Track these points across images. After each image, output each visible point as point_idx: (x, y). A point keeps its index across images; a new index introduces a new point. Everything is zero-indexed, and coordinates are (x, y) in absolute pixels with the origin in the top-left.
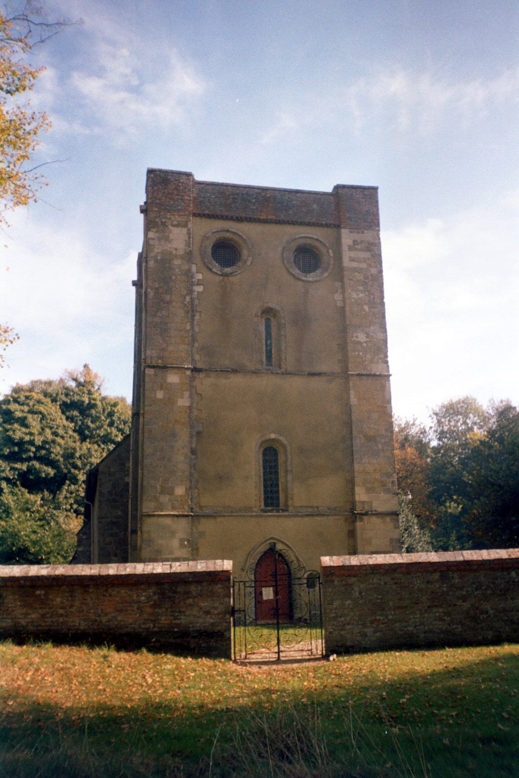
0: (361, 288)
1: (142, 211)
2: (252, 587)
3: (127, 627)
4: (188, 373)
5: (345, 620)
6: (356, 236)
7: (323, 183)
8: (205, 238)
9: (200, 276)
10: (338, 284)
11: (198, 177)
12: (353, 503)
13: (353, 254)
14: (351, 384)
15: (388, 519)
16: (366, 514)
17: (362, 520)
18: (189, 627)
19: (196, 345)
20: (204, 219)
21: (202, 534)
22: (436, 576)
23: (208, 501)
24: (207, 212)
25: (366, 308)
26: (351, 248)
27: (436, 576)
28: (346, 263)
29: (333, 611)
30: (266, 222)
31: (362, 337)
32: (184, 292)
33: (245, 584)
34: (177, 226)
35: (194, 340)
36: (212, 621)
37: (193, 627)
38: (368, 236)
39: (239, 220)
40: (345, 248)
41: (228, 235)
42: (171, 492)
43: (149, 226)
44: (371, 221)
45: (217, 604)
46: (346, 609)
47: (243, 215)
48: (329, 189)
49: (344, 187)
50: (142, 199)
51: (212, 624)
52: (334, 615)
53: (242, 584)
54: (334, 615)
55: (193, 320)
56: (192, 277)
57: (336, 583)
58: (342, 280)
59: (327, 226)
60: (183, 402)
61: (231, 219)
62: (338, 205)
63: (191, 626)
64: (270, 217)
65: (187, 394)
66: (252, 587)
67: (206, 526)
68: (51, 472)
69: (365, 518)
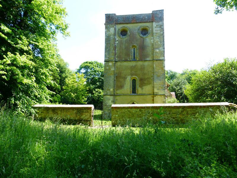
0: (158, 38)
1: (105, 25)
3: (25, 139)
4: (114, 62)
6: (157, 24)
7: (149, 11)
8: (119, 29)
9: (117, 39)
10: (152, 37)
11: (117, 15)
12: (154, 92)
13: (156, 29)
14: (154, 63)
15: (163, 96)
16: (157, 95)
17: (155, 97)
19: (116, 56)
20: (118, 25)
21: (117, 100)
22: (139, 110)
23: (119, 92)
24: (119, 23)
25: (159, 43)
26: (155, 27)
27: (139, 110)
28: (154, 31)
30: (134, 23)
31: (157, 51)
32: (113, 43)
34: (112, 27)
35: (115, 54)
38: (161, 23)
39: (127, 24)
40: (154, 27)
41: (125, 28)
42: (109, 90)
43: (106, 28)
44: (161, 19)
47: (128, 22)
48: (151, 12)
49: (154, 11)
50: (104, 22)
55: (115, 50)
56: (116, 39)
58: (153, 36)
59: (150, 22)
60: (113, 69)
61: (125, 24)
62: (153, 17)
64: (135, 22)
65: (113, 67)
67: (117, 98)
68: (96, 90)
69: (157, 96)
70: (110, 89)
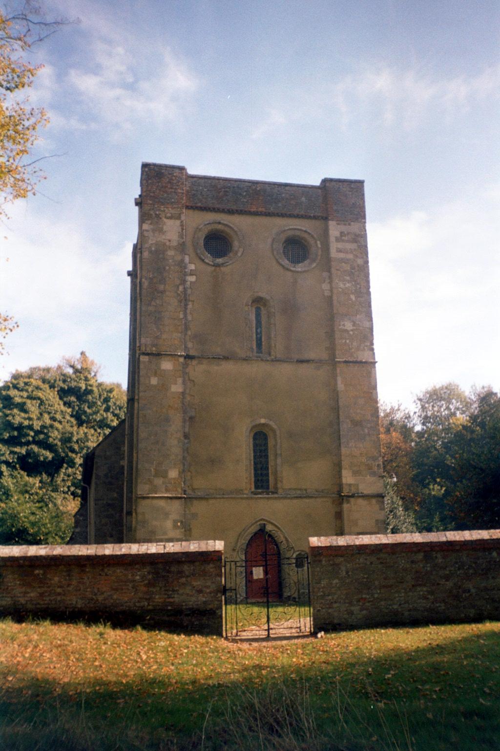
2: (243, 567)
5: (333, 599)
18: (182, 605)
29: (321, 590)
33: (236, 564)
36: (204, 599)
37: (186, 605)
45: (209, 583)
46: (333, 588)
51: (205, 603)
52: (322, 593)
53: (233, 563)
54: (322, 593)
57: (324, 562)
63: (184, 604)
66: (243, 567)
70: (166, 472)
